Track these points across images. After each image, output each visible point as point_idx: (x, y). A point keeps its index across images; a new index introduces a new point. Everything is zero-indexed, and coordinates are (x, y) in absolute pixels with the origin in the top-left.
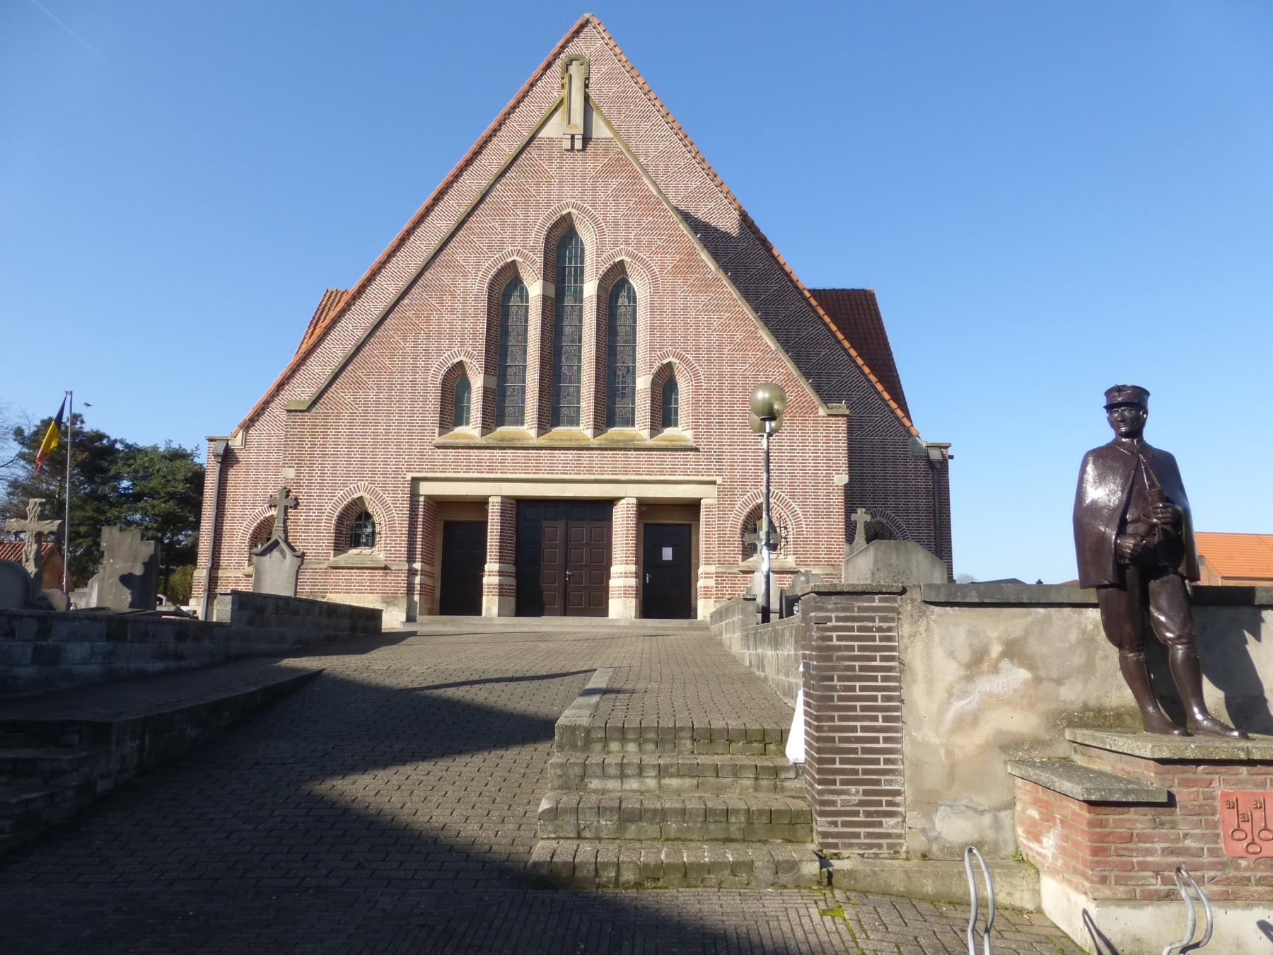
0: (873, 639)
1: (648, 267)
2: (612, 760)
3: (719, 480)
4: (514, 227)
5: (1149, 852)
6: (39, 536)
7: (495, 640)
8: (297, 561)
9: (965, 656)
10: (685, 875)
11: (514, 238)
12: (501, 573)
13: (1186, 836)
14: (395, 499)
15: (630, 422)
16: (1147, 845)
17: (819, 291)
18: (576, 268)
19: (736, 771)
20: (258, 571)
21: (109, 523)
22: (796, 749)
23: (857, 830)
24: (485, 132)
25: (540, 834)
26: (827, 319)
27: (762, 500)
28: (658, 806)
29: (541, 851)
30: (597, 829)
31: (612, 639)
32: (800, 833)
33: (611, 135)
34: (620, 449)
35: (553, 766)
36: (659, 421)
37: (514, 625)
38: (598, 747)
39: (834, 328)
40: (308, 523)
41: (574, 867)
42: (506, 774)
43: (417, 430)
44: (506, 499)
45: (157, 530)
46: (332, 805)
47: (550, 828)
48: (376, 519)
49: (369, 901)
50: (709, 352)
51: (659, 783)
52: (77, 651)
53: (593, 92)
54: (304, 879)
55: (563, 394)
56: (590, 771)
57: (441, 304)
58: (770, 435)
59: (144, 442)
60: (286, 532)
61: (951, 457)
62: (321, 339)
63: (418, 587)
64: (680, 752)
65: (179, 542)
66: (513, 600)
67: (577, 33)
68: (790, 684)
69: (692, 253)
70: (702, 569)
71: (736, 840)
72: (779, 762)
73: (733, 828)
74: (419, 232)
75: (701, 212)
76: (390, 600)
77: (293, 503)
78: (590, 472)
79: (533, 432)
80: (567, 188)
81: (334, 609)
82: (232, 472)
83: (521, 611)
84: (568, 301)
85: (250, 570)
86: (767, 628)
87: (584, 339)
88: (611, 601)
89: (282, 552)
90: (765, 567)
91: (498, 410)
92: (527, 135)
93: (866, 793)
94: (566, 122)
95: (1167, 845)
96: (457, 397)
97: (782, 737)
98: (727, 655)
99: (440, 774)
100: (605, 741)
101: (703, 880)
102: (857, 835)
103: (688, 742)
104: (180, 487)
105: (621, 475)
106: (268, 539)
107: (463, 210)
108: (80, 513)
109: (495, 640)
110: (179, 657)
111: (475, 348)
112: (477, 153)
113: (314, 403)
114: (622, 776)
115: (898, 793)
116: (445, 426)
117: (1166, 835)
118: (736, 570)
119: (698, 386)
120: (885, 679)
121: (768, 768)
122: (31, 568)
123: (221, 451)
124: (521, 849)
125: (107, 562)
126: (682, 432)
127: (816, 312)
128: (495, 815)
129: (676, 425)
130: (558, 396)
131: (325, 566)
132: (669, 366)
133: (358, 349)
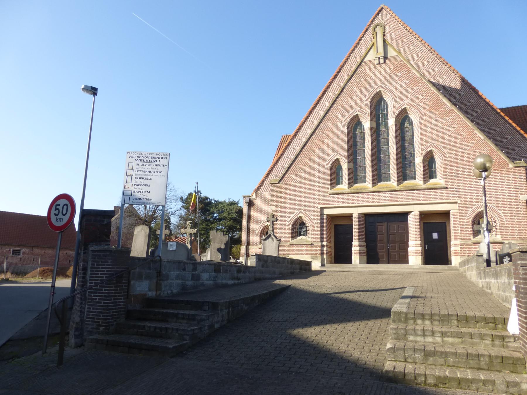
1: (417, 109)
2: (419, 328)
3: (459, 201)
4: (356, 100)
6: (191, 234)
7: (357, 275)
8: (278, 242)
10: (459, 383)
11: (356, 105)
12: (360, 246)
14: (314, 216)
15: (388, 179)
17: (505, 109)
18: (384, 114)
19: (482, 336)
20: (264, 247)
21: (211, 229)
22: (514, 327)
24: (341, 64)
25: (387, 358)
26: (510, 121)
27: (483, 208)
28: (443, 350)
29: (388, 366)
30: (414, 358)
31: (411, 274)
32: (519, 368)
33: (397, 54)
34: (410, 190)
35: (392, 329)
36: (428, 176)
37: (366, 268)
38: (412, 322)
39: (514, 125)
40: (281, 228)
41: (405, 374)
42: (370, 331)
43: (321, 188)
44: (360, 214)
45: (227, 232)
46: (299, 339)
47: (392, 356)
48: (307, 225)
49: (317, 380)
50: (450, 143)
51: (442, 339)
52: (205, 276)
53: (387, 37)
54: (290, 368)
55: (382, 168)
56: (408, 332)
57: (328, 135)
58: (485, 179)
59: (221, 199)
60: (273, 231)
62: (282, 155)
63: (325, 252)
64: (451, 326)
65: (235, 236)
66: (365, 257)
67: (378, 14)
68: (506, 296)
69: (438, 100)
70: (453, 242)
71: (484, 369)
72: (504, 333)
73: (482, 363)
74: (317, 108)
75: (442, 81)
76: (314, 257)
77: (275, 220)
78: (396, 201)
79: (370, 185)
80: (378, 80)
81: (293, 261)
82: (252, 209)
83: (369, 262)
84: (382, 128)
85: (260, 246)
86: (488, 269)
87: (390, 144)
88: (409, 257)
89: (272, 239)
90: (486, 241)
91: (354, 177)
92: (359, 61)
94: (376, 52)
96: (337, 173)
97: (505, 321)
98: (470, 282)
99: (341, 329)
100: (415, 319)
101: (469, 386)
103: (456, 322)
104: (234, 215)
105: (412, 201)
106: (267, 234)
107: (334, 97)
108: (202, 226)
109: (357, 275)
110: (238, 279)
111: (343, 152)
112: (339, 72)
113: (281, 180)
114: (424, 335)
116: (333, 186)
118: (470, 242)
119: (445, 160)
121: (498, 336)
122: (189, 246)
123: (248, 201)
124: (379, 364)
125: (213, 243)
126: (438, 180)
127: (504, 119)
128: (367, 349)
129: (436, 178)
130: (380, 169)
131: (288, 244)
132: (431, 151)
133: (296, 157)
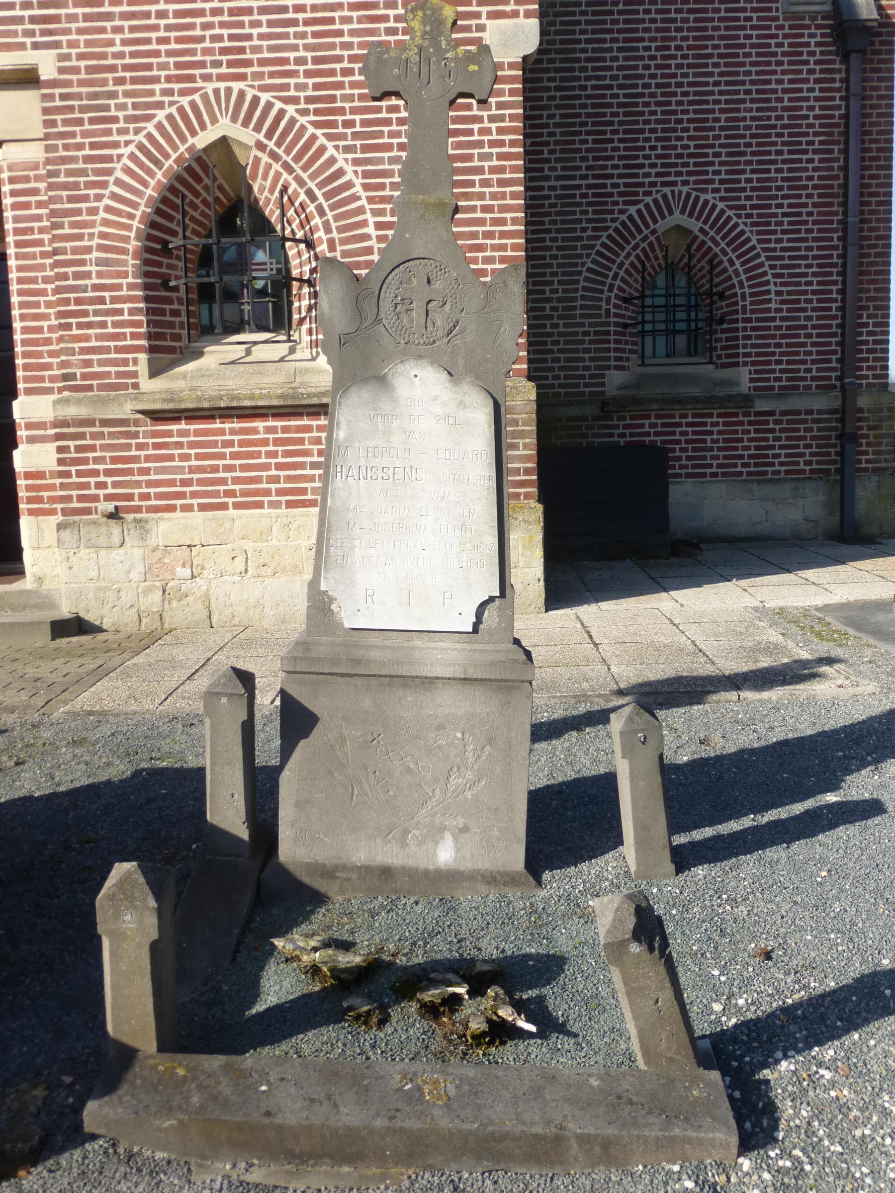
3: (47, 65)
118: (126, 409)
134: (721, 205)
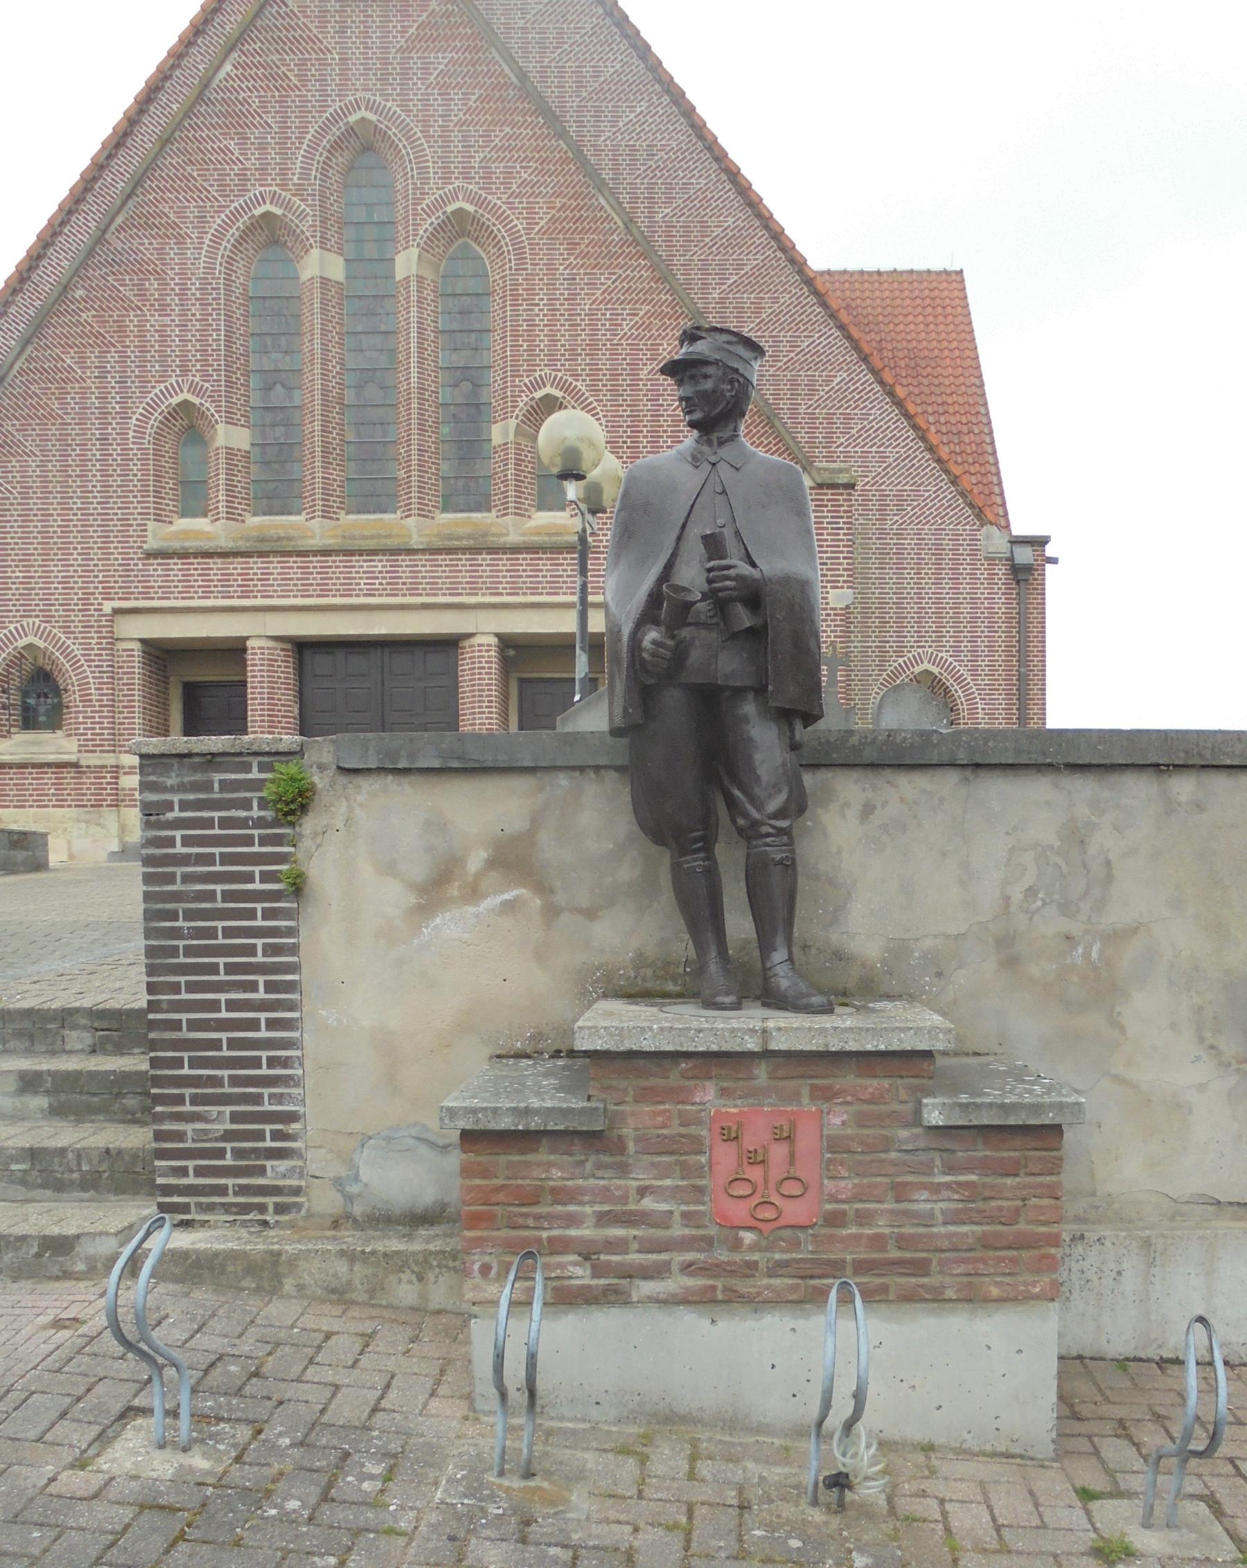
0: (249, 841)
4: (263, 147)
5: (572, 1220)
9: (419, 870)
11: (262, 170)
13: (643, 1192)
16: (572, 1208)
23: (223, 1181)
61: (1054, 561)
78: (413, 591)
93: (235, 1117)
95: (607, 1208)
102: (221, 1190)
111: (206, 376)
115: (292, 1117)
117: (606, 1189)
120: (267, 914)
134: (950, 659)
